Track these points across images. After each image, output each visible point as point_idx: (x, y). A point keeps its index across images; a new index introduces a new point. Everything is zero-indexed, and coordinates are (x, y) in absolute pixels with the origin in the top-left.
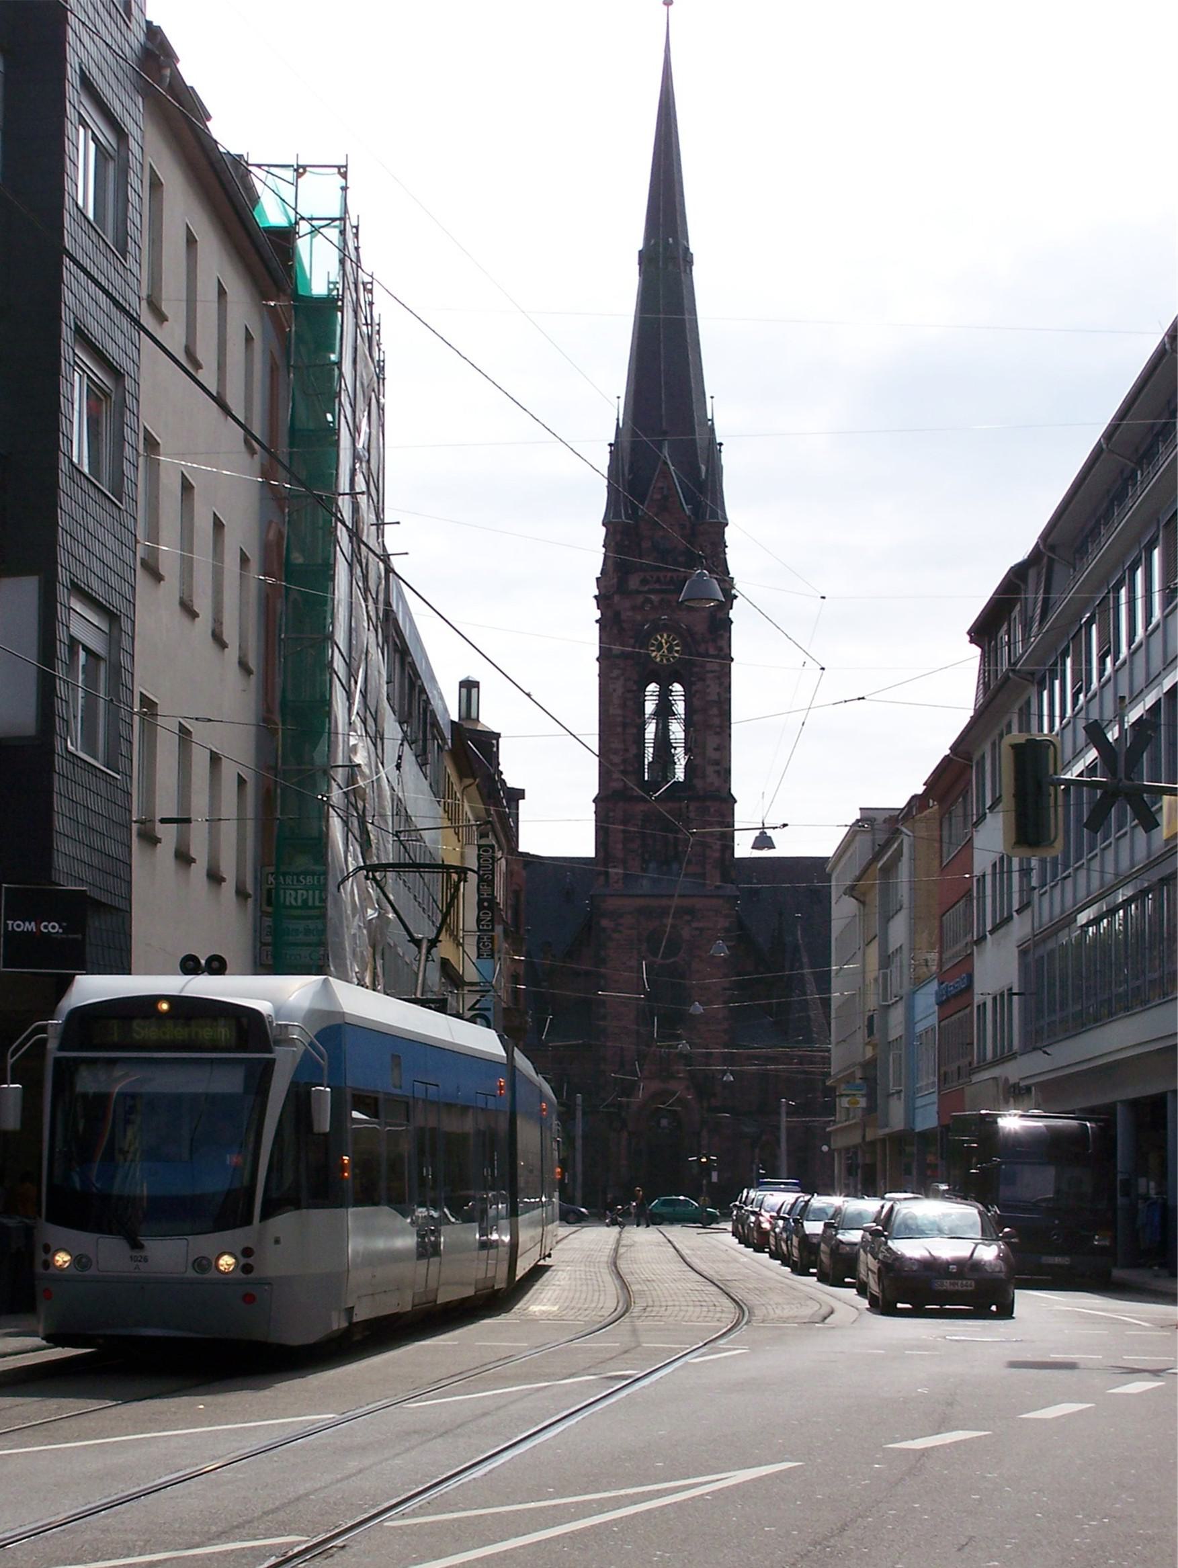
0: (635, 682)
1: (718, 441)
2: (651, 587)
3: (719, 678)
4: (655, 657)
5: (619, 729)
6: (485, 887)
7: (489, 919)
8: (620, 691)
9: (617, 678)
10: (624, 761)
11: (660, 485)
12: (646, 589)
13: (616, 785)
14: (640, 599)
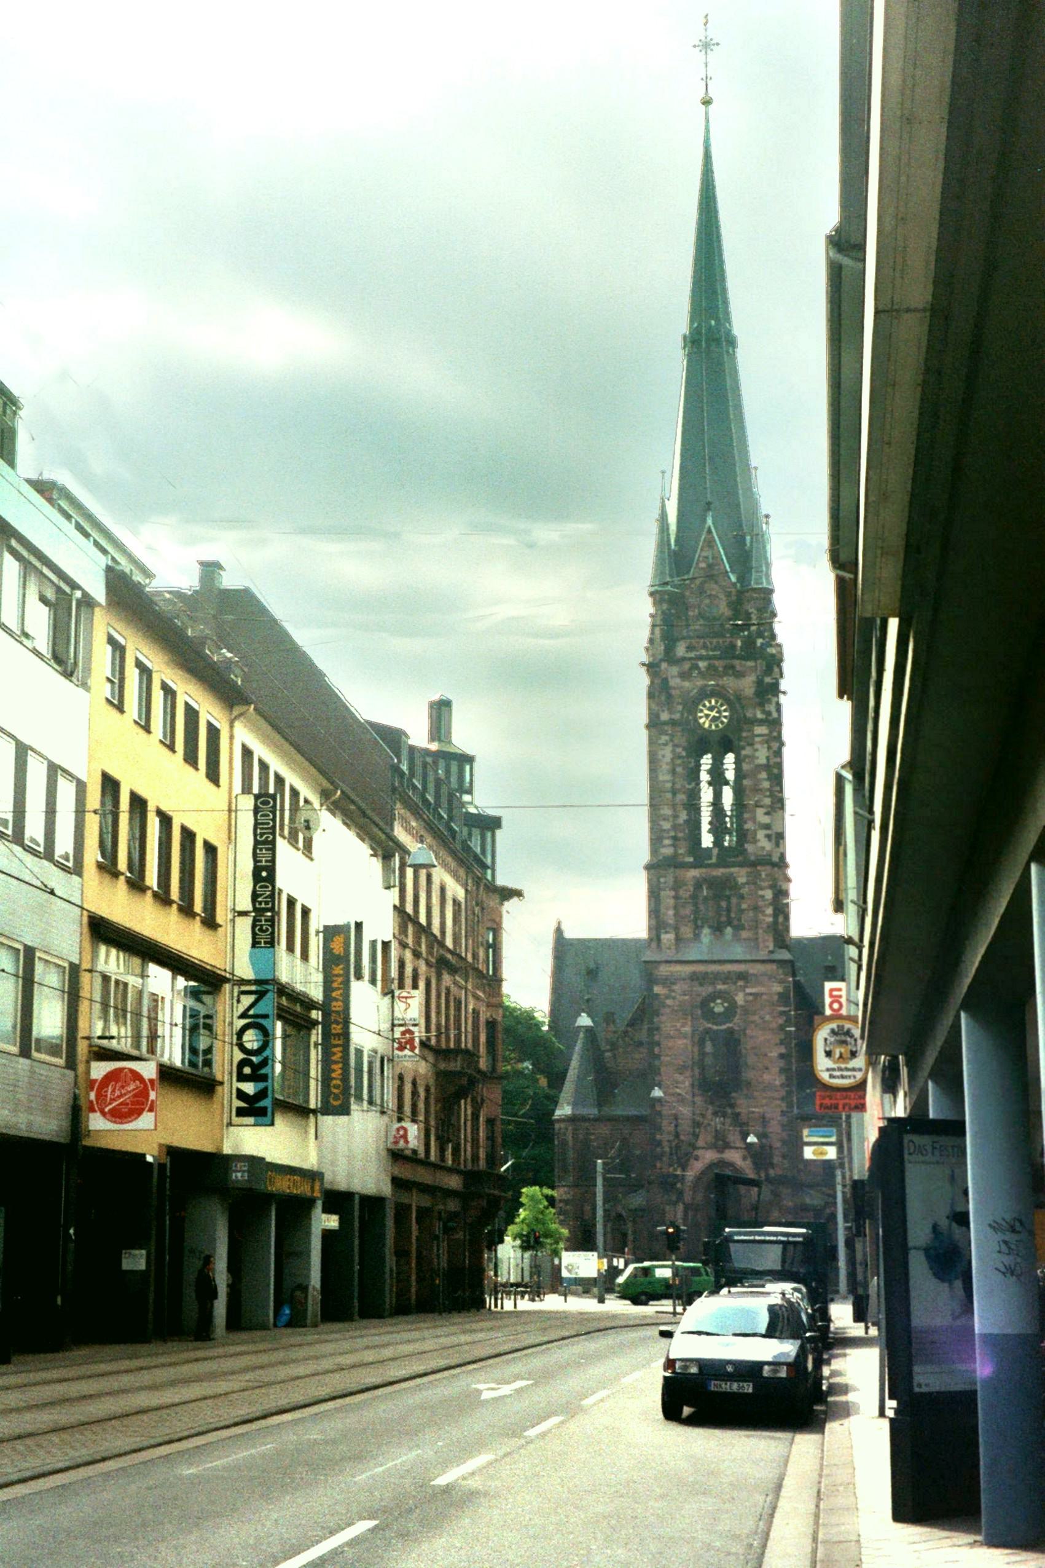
0: (684, 749)
1: (764, 512)
2: (698, 653)
3: (767, 742)
4: (704, 723)
5: (669, 795)
6: (264, 851)
7: (268, 893)
8: (669, 756)
9: (665, 745)
10: (675, 827)
11: (704, 554)
12: (692, 655)
13: (668, 851)
14: (687, 666)
